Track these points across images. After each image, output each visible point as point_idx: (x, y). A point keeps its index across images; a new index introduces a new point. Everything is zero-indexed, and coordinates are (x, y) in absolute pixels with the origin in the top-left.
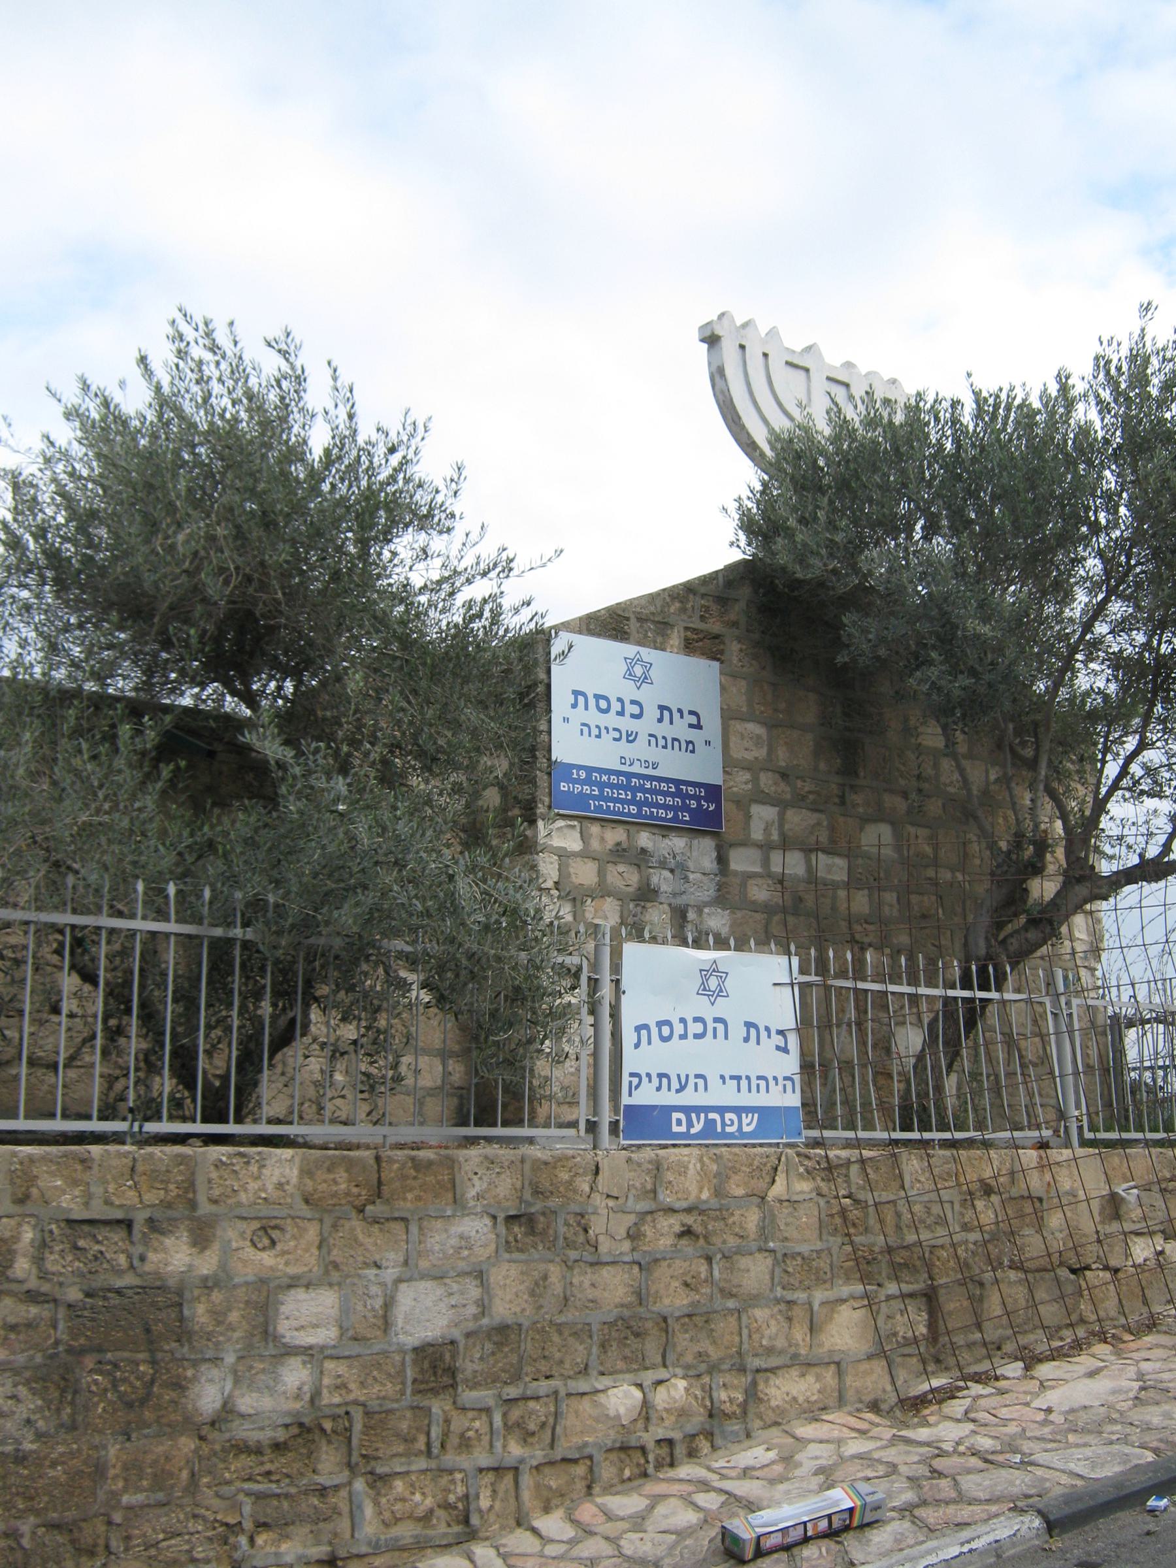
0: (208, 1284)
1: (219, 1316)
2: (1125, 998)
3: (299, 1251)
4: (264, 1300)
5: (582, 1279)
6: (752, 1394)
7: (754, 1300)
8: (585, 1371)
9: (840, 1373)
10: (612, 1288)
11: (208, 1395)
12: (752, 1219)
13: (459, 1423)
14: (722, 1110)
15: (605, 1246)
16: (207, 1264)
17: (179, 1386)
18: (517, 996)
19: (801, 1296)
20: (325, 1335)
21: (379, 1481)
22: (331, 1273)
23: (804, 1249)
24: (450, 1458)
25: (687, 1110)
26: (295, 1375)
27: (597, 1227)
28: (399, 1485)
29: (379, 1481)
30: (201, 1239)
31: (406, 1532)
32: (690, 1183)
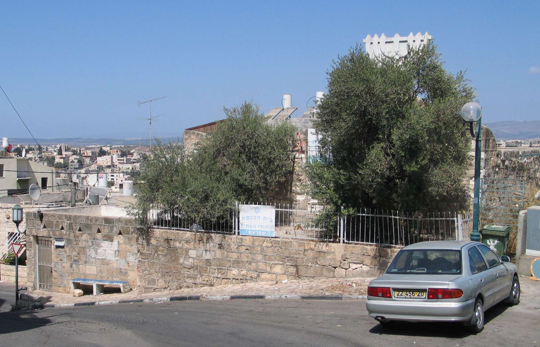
0: (181, 248)
1: (182, 252)
2: (117, 224)
3: (191, 245)
4: (187, 251)
5: (230, 254)
6: (258, 276)
7: (260, 261)
8: (230, 267)
9: (277, 276)
10: (235, 256)
11: (181, 261)
12: (259, 249)
13: (212, 270)
14: (258, 231)
15: (233, 250)
16: (180, 246)
17: (178, 259)
18: (255, 121)
19: (268, 262)
20: (195, 256)
21: (201, 276)
22: (195, 248)
23: (269, 255)
24: (210, 275)
25: (252, 231)
26: (191, 260)
27: (232, 247)
28: (204, 277)
29: (201, 276)
30: (180, 243)
31: (205, 282)
32: (247, 241)
